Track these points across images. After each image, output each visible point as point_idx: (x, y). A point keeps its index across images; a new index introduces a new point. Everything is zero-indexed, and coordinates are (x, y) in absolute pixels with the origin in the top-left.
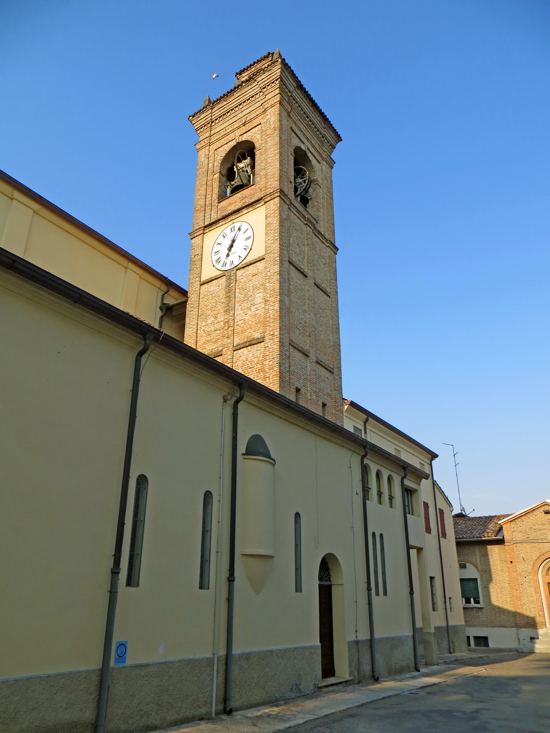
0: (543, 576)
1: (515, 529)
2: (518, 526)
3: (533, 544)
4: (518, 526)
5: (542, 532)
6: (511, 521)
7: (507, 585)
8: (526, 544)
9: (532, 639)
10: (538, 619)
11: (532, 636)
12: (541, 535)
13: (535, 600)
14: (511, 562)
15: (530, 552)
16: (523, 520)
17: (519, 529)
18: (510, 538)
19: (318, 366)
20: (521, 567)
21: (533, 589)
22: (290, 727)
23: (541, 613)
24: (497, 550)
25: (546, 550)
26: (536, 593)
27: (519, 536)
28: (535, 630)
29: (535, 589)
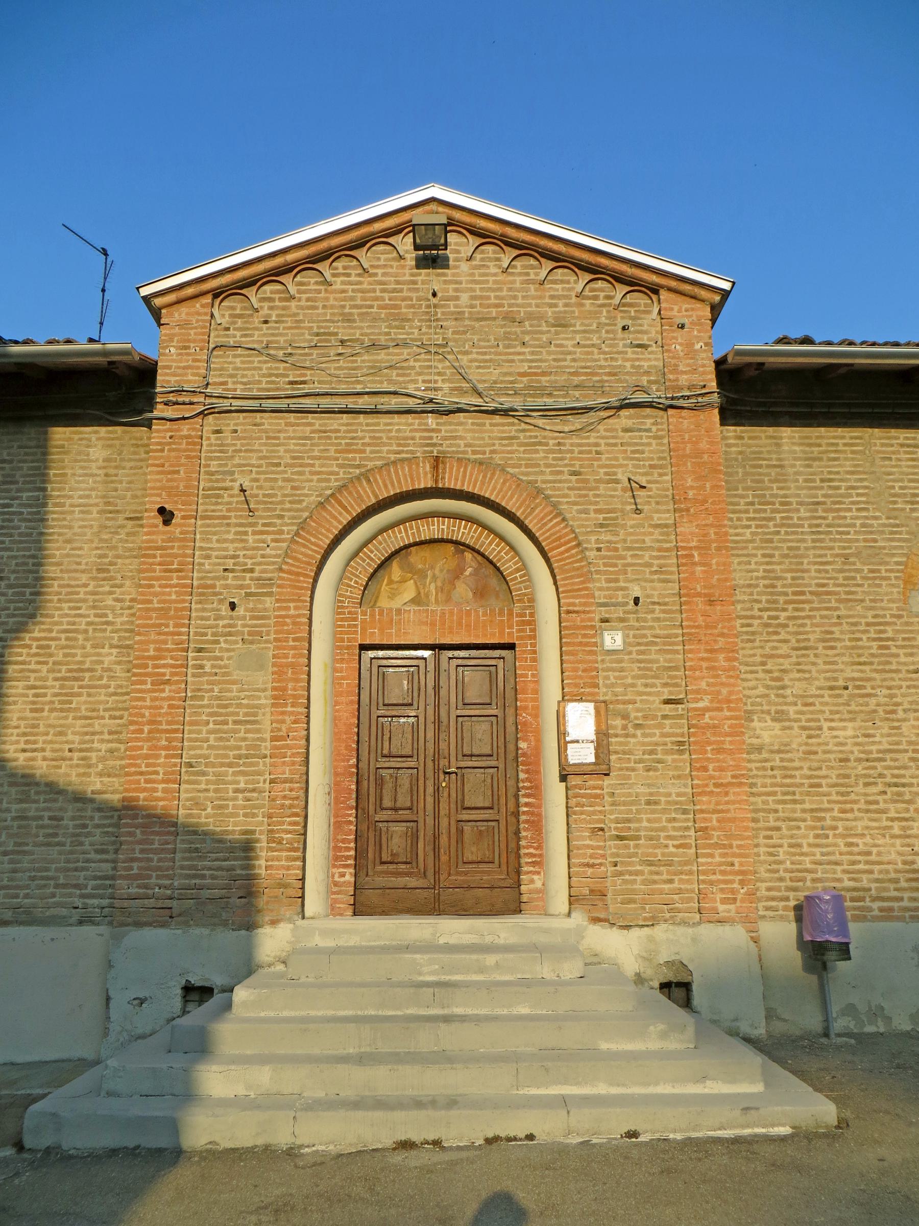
0: (338, 608)
1: (235, 337)
2: (256, 320)
3: (317, 421)
4: (256, 320)
5: (382, 355)
6: (217, 294)
7: (110, 656)
8: (280, 421)
9: (196, 993)
10: (268, 864)
11: (196, 980)
12: (376, 370)
13: (266, 747)
14: (166, 515)
15: (303, 463)
16: (293, 289)
17: (257, 338)
18: (191, 381)
19: (506, 640)
20: (213, 542)
21: (264, 678)
22: (406, 1145)
23: (286, 830)
24: (98, 453)
25: (387, 452)
26: (279, 697)
27: (240, 375)
28: (228, 937)
29: (279, 673)
